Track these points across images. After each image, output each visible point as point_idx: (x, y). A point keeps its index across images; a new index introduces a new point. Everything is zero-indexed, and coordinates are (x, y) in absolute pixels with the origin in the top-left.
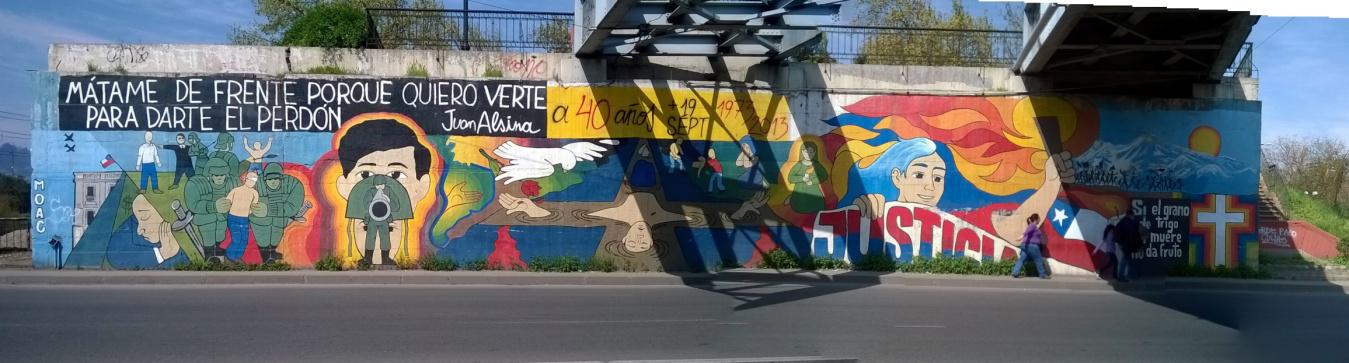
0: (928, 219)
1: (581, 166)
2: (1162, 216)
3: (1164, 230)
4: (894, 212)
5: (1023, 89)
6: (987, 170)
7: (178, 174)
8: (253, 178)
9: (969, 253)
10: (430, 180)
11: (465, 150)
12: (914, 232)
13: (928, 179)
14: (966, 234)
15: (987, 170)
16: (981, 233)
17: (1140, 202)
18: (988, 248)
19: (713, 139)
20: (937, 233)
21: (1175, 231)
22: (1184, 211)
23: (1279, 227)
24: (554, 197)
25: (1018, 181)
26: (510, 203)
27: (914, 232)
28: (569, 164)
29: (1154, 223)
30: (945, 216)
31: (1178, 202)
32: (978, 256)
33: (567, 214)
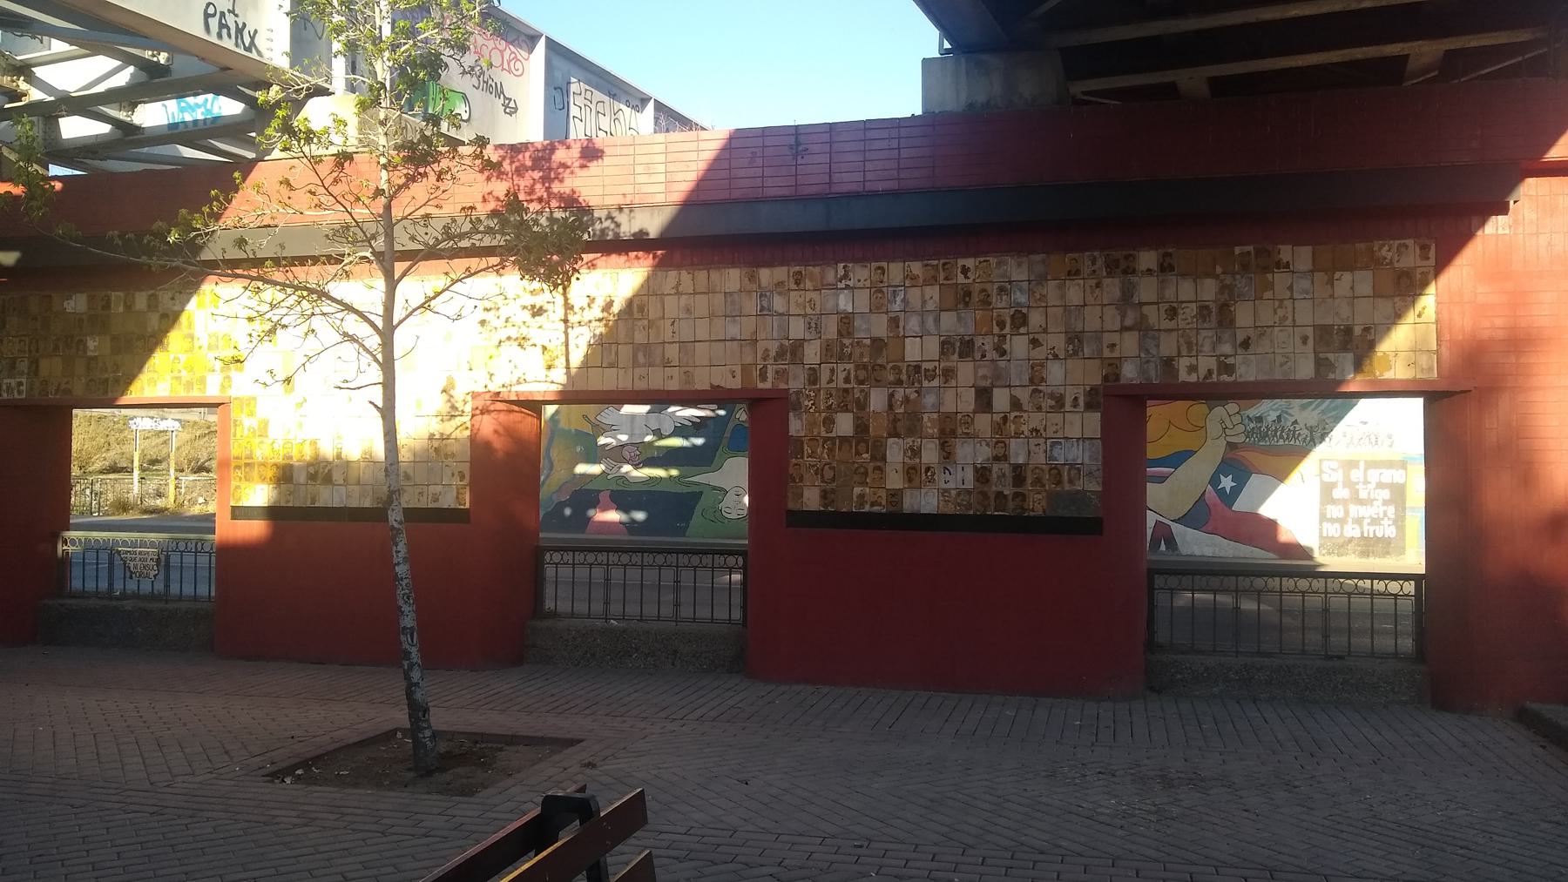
2: (1366, 482)
3: (1368, 502)
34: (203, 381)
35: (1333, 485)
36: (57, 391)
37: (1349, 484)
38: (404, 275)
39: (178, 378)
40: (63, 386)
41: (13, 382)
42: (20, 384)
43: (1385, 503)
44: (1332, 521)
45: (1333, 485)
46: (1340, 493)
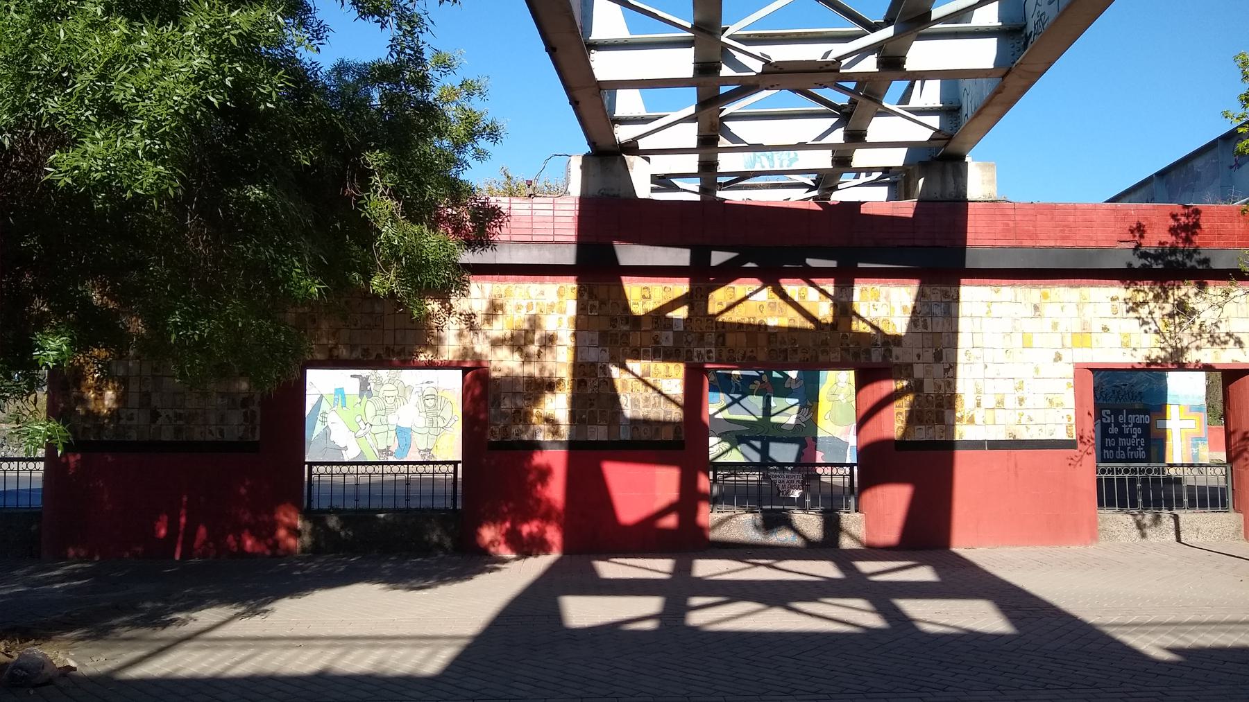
2: (1128, 423)
3: (1129, 436)
5: (681, 400)
7: (361, 396)
8: (414, 399)
17: (1109, 412)
19: (972, 295)
21: (1139, 436)
22: (1145, 419)
23: (812, 368)
29: (1121, 430)
31: (1140, 412)
34: (868, 352)
35: (1109, 425)
36: (743, 358)
37: (1117, 424)
38: (823, 292)
39: (847, 350)
40: (748, 354)
41: (703, 351)
42: (710, 352)
43: (1139, 436)
44: (1108, 448)
45: (1109, 425)
46: (1113, 430)
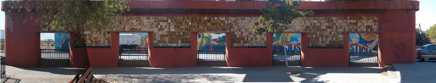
0: (357, 45)
1: (223, 37)
4: (297, 44)
6: (366, 37)
9: (364, 51)
10: (200, 39)
11: (206, 35)
12: (355, 47)
13: (357, 39)
14: (363, 47)
15: (366, 37)
16: (365, 47)
18: (367, 49)
20: (358, 47)
24: (219, 41)
25: (372, 39)
26: (212, 42)
27: (355, 47)
28: (221, 37)
30: (360, 44)
32: (365, 51)
33: (221, 44)
